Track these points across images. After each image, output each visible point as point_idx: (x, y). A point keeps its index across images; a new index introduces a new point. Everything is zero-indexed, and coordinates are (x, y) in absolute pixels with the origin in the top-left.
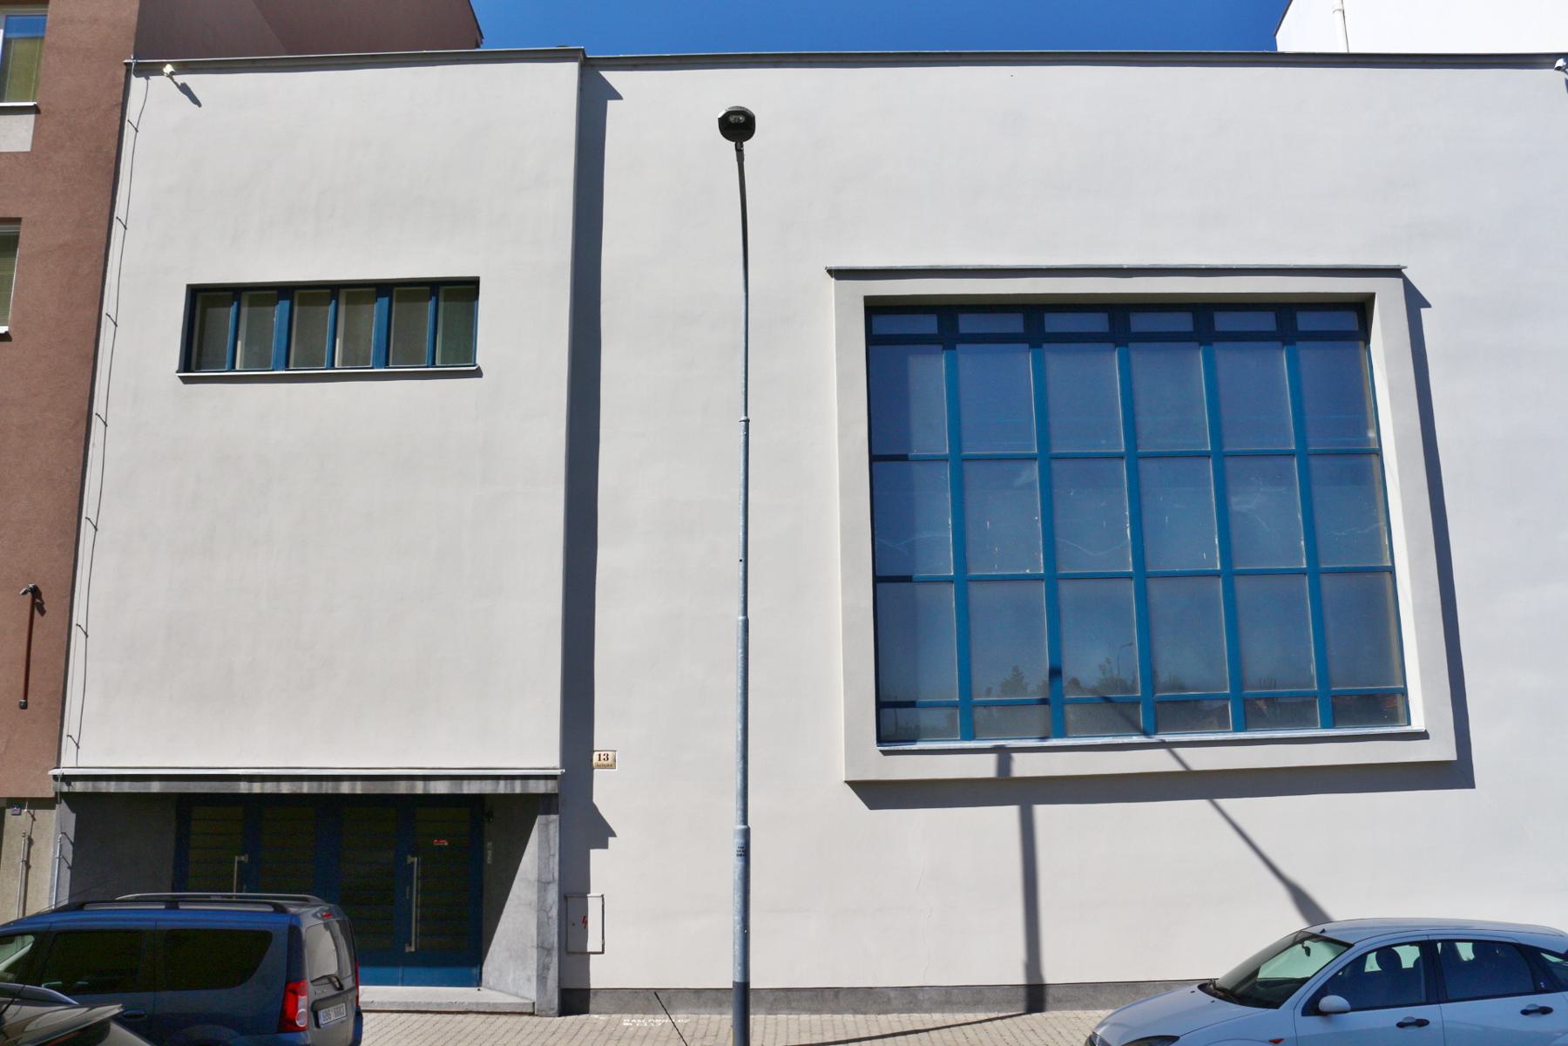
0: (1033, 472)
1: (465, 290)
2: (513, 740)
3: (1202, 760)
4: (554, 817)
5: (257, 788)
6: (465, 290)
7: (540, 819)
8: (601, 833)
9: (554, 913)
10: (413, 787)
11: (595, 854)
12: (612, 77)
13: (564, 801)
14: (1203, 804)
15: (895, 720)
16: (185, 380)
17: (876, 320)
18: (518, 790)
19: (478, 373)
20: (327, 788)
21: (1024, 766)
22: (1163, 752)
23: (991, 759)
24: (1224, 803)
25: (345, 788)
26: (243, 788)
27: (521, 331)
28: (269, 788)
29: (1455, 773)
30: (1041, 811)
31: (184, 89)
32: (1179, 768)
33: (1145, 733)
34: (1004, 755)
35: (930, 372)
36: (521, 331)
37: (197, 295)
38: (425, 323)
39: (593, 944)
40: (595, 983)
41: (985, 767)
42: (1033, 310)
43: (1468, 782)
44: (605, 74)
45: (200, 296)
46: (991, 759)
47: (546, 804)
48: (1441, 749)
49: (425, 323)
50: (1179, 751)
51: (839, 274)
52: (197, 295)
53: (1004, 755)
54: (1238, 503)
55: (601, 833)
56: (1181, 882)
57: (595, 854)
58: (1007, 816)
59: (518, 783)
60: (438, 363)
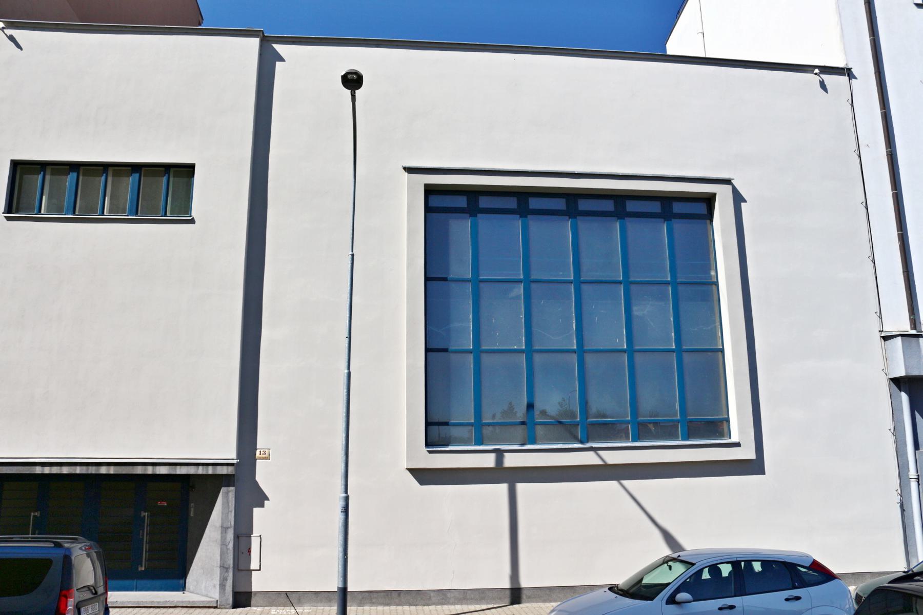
0: (520, 290)
1: (188, 170)
2: (211, 443)
3: (613, 458)
4: (232, 489)
5: (47, 470)
6: (188, 170)
7: (223, 490)
8: (260, 498)
9: (231, 546)
10: (145, 470)
11: (257, 511)
12: (280, 48)
13: (238, 480)
14: (614, 483)
15: (436, 433)
16: (8, 219)
17: (431, 198)
18: (210, 472)
19: (192, 221)
20: (92, 470)
21: (510, 461)
22: (591, 453)
23: (492, 456)
24: (625, 482)
25: (103, 470)
26: (38, 470)
27: (219, 196)
28: (55, 470)
29: (755, 467)
30: (522, 488)
31: (11, 38)
32: (600, 463)
33: (582, 442)
34: (500, 454)
35: (461, 230)
36: (219, 196)
37: (17, 167)
38: (160, 190)
39: (254, 565)
40: (255, 588)
41: (488, 461)
42: (666, 199)
43: (762, 471)
44: (277, 47)
45: (19, 167)
46: (492, 456)
47: (227, 480)
48: (747, 453)
49: (160, 190)
50: (601, 453)
51: (410, 170)
52: (17, 167)
53: (500, 454)
54: (637, 311)
55: (260, 498)
56: (604, 526)
57: (257, 511)
58: (503, 488)
59: (210, 468)
60: (168, 214)
